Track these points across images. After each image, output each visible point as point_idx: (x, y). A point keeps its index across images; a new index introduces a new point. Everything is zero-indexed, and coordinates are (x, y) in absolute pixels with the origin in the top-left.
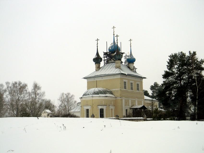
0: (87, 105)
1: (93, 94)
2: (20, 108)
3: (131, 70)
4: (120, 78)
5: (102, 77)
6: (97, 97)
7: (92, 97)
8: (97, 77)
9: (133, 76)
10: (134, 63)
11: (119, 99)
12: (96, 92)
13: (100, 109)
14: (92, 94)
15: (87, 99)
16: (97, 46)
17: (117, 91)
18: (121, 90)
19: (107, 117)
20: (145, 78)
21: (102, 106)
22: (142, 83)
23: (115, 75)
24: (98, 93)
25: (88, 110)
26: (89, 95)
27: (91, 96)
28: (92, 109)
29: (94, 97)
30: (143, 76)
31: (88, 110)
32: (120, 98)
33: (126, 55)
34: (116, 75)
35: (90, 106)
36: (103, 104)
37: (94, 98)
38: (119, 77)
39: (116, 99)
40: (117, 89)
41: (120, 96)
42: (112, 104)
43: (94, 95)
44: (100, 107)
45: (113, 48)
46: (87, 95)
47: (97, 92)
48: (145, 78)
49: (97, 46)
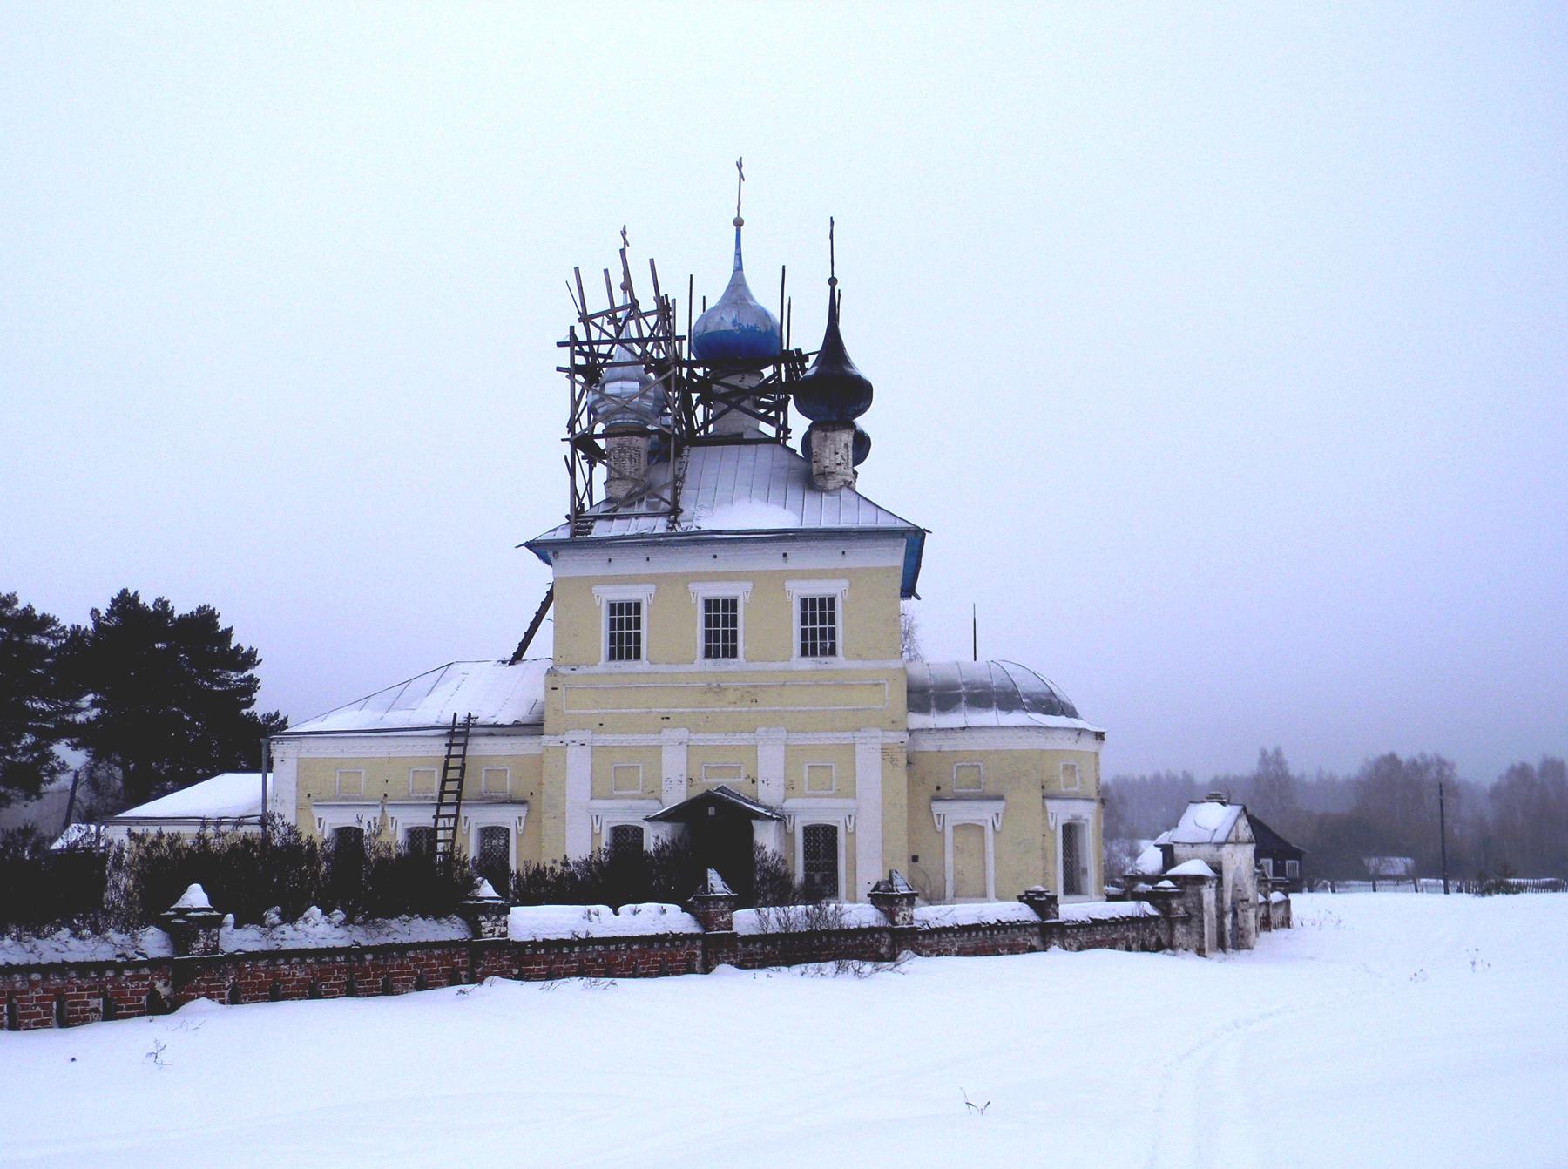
13: (805, 828)
44: (1061, 813)
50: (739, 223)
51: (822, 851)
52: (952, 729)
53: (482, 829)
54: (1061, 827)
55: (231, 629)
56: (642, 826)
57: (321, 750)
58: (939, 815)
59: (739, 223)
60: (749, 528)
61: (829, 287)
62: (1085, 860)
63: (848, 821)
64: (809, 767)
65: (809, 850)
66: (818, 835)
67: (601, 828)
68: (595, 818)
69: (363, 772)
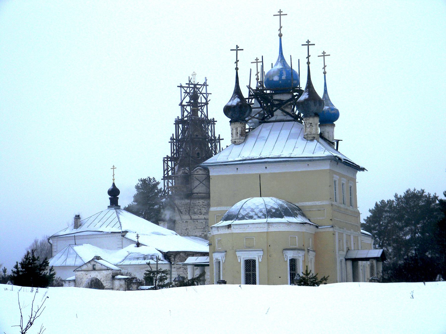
0: (249, 248)
1: (265, 216)
2: (437, 255)
3: (331, 143)
4: (330, 170)
5: (266, 165)
6: (282, 225)
7: (266, 225)
8: (244, 164)
9: (294, 161)
10: (334, 125)
11: (327, 230)
12: (274, 211)
13: (290, 260)
14: (260, 215)
15: (248, 231)
16: (237, 69)
17: (320, 209)
18: (332, 205)
19: (260, 284)
20: (363, 169)
21: (296, 252)
22: (354, 180)
23: (313, 160)
24: (280, 213)
25: (293, 263)
26: (251, 217)
27: (264, 220)
28: (268, 258)
29: (275, 225)
30: (361, 166)
31: (293, 263)
32: (331, 229)
33: (190, 81)
34: (321, 160)
35: (262, 252)
36: (297, 246)
37: (273, 229)
38: (326, 166)
39: (318, 230)
40: (318, 203)
41: (331, 223)
42: (297, 245)
43: (270, 220)
44: (290, 255)
45: (284, 77)
46: (243, 218)
47: (277, 210)
48: (363, 169)
49: (237, 69)
50: (280, 35)
51: (252, 268)
52: (272, 223)
53: (246, 260)
54: (289, 260)
55: (376, 202)
56: (255, 259)
57: (271, 230)
58: (239, 256)
59: (280, 35)
60: (309, 156)
61: (307, 65)
62: (298, 270)
63: (223, 259)
64: (290, 237)
65: (247, 269)
66: (253, 264)
67: (241, 260)
68: (259, 256)
69: (297, 237)
